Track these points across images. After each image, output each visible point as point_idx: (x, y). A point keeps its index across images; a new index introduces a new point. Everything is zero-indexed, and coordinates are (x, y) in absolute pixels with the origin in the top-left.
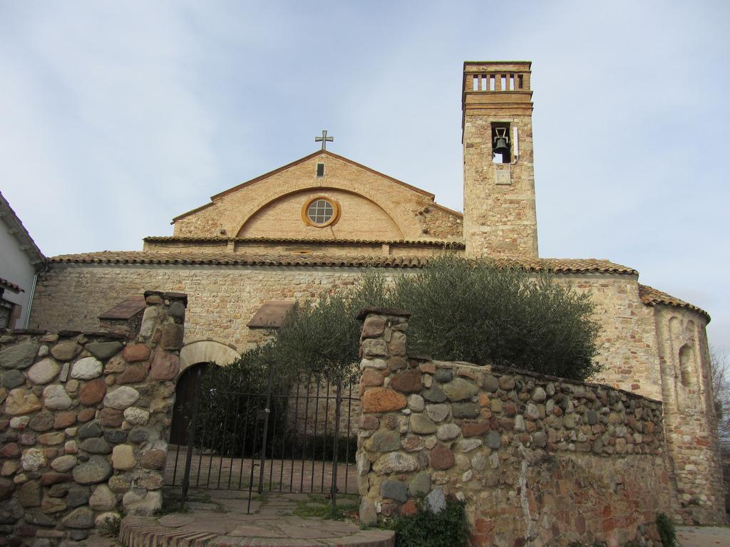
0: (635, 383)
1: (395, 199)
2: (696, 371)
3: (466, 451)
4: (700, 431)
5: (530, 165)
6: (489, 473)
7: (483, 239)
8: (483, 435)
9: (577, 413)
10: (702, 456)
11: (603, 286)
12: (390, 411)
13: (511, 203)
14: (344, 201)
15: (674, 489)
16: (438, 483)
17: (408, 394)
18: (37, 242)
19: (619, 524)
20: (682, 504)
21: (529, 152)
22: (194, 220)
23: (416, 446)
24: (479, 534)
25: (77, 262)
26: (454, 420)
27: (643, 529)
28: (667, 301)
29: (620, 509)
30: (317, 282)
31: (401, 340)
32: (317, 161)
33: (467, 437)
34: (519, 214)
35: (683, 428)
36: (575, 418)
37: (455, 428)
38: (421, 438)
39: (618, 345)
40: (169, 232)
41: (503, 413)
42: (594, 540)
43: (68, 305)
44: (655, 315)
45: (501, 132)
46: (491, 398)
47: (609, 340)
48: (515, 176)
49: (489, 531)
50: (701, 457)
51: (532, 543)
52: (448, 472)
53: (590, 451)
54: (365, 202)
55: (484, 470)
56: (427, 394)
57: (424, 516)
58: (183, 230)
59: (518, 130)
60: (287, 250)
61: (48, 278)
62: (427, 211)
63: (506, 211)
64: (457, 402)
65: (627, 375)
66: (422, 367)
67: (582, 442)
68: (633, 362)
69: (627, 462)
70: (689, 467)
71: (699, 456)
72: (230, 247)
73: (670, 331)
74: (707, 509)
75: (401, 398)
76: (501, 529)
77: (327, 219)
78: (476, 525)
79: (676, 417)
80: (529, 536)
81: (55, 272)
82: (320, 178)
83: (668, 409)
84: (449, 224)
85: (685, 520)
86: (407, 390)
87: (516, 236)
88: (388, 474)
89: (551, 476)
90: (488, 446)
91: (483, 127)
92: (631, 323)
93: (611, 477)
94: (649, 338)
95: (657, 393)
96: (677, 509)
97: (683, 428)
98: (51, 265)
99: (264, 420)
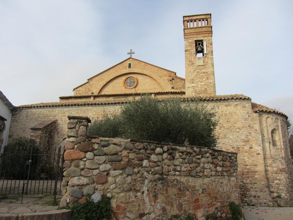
0: (251, 146)
1: (160, 75)
2: (280, 140)
3: (113, 176)
4: (282, 166)
5: (211, 57)
6: (125, 185)
7: (192, 89)
8: (123, 169)
9: (182, 158)
10: (283, 177)
11: (236, 105)
12: (76, 159)
13: (204, 73)
14: (140, 78)
15: (269, 191)
16: (98, 189)
17: (86, 152)
18: (10, 101)
19: (203, 207)
20: (273, 197)
21: (211, 51)
22: (81, 89)
23: (88, 174)
24: (119, 211)
25: (26, 107)
26: (108, 163)
27: (219, 209)
28: (265, 110)
29: (204, 200)
30: (117, 110)
31: (83, 129)
32: (128, 62)
33: (114, 170)
34: (208, 78)
35: (273, 165)
36: (180, 161)
37: (108, 166)
38: (91, 170)
39: (243, 130)
40: (72, 94)
41: (136, 159)
42: (188, 214)
43: (23, 125)
44: (259, 116)
45: (199, 44)
46: (129, 153)
47: (239, 128)
48: (205, 62)
49: (124, 210)
50: (282, 177)
51: (150, 215)
52: (104, 185)
53: (189, 175)
54: (148, 77)
55: (123, 184)
56: (95, 152)
57: (89, 203)
58: (77, 93)
59: (206, 42)
60: (114, 98)
61: (16, 114)
62: (173, 79)
63: (202, 77)
64: (110, 155)
65: (247, 143)
66: (93, 140)
67: (184, 171)
68: (250, 137)
69: (211, 180)
70: (276, 182)
71: (281, 177)
72: (92, 98)
73: (266, 123)
74: (285, 199)
75: (82, 154)
76: (130, 209)
77: (133, 85)
78: (116, 208)
79: (270, 160)
80: (147, 212)
81: (18, 112)
82: (130, 69)
83: (266, 157)
84: (182, 84)
85: (274, 204)
86: (85, 150)
87: (206, 87)
88: (73, 186)
89: (163, 186)
90: (126, 174)
91: (191, 43)
92: (248, 120)
93: (201, 186)
94: (257, 127)
95: (260, 150)
96: (270, 200)
97: (273, 165)
98: (17, 109)
99: (29, 165)
